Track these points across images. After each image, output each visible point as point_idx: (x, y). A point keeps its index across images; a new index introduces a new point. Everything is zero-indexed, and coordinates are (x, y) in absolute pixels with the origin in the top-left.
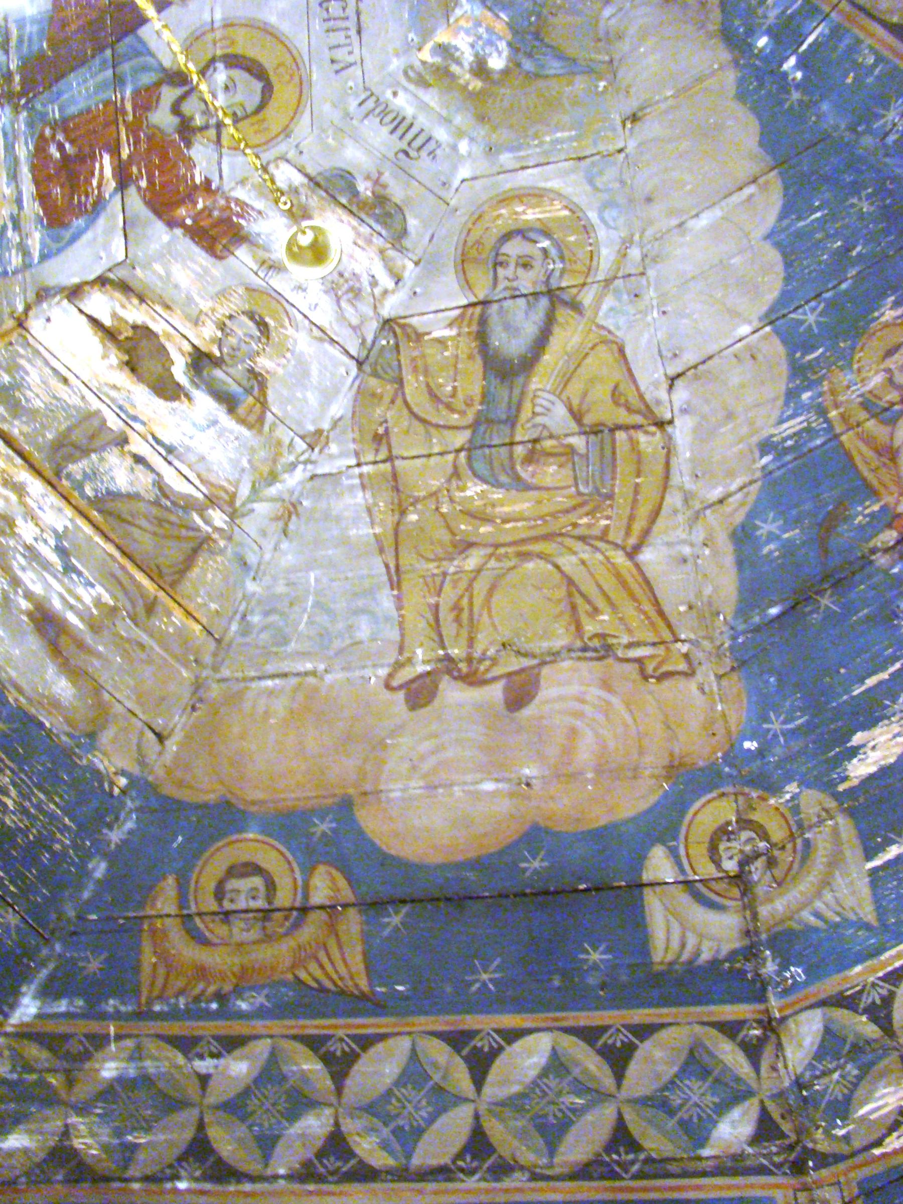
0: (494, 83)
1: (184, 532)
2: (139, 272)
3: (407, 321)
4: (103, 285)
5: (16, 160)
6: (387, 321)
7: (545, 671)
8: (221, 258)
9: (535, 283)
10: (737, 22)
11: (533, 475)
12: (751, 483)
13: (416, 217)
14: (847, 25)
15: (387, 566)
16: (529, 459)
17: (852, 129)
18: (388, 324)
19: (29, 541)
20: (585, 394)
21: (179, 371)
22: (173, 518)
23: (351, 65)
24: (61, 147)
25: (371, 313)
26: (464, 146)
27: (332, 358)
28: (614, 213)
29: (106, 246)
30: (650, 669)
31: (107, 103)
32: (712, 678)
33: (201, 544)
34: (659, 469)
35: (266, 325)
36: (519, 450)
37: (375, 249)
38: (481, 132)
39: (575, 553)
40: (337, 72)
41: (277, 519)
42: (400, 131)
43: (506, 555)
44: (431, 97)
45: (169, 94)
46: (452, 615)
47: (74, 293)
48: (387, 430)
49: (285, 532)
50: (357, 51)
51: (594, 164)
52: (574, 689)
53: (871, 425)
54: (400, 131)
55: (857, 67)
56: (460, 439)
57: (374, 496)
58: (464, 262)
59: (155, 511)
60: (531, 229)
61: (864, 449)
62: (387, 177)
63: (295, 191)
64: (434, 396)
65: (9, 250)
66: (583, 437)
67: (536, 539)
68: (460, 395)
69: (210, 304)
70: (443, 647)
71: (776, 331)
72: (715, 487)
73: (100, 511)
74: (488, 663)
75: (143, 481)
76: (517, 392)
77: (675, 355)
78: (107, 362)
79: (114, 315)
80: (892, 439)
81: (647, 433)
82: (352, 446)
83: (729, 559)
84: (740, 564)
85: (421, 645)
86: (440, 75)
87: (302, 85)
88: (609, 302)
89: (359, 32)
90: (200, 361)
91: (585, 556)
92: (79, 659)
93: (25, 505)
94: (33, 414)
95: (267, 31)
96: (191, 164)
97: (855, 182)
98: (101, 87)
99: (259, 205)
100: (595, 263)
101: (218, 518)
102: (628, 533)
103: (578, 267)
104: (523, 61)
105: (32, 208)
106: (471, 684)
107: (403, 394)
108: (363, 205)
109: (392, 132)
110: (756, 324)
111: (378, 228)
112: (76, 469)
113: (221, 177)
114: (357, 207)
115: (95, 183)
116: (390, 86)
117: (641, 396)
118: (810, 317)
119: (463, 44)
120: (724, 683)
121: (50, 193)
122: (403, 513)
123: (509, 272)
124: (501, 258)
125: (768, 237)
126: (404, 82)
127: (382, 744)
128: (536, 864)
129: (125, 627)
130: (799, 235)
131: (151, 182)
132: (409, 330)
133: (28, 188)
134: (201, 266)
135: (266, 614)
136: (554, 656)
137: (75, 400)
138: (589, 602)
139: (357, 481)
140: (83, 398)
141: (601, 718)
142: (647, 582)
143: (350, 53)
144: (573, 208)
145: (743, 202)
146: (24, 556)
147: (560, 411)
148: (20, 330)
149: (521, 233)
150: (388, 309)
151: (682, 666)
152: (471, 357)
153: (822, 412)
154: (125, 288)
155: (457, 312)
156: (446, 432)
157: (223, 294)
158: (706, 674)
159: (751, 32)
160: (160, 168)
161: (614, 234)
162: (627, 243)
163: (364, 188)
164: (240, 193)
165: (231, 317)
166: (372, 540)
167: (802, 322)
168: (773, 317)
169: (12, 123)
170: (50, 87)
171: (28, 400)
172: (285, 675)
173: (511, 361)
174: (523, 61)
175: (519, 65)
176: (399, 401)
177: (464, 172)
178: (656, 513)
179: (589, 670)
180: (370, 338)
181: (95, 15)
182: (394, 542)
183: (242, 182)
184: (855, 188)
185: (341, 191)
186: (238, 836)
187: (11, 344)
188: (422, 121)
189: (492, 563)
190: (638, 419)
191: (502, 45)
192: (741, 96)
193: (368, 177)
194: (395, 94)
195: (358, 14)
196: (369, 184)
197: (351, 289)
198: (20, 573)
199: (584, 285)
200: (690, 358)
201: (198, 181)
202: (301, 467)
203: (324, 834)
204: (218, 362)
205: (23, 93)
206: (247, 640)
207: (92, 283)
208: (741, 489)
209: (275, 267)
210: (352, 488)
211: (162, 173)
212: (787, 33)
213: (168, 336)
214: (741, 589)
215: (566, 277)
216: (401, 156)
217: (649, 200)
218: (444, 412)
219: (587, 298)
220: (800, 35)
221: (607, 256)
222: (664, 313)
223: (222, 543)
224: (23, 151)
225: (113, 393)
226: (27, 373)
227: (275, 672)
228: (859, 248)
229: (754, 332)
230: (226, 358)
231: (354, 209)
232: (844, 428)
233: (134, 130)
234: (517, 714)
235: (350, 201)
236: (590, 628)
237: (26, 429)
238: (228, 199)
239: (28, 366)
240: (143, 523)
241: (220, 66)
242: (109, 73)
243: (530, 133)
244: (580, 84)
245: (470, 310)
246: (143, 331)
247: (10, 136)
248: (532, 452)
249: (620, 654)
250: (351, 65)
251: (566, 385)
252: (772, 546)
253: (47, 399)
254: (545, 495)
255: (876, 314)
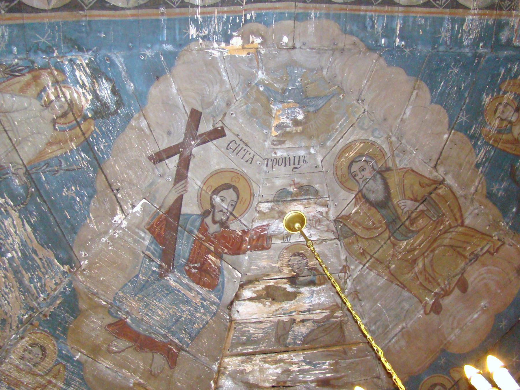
0: (306, 123)
1: (333, 326)
2: (249, 274)
3: (341, 215)
4: (243, 287)
5: (187, 285)
6: (335, 221)
7: (465, 275)
8: (269, 248)
9: (370, 173)
10: (370, 42)
11: (417, 227)
12: (481, 179)
13: (316, 184)
14: (407, 15)
15: (398, 285)
16: (412, 224)
17: (433, 48)
18: (336, 221)
19: (297, 369)
20: (413, 193)
21: (289, 288)
22: (327, 326)
23: (253, 157)
24: (195, 268)
25: (328, 222)
26: (312, 151)
27: (329, 244)
28: (378, 132)
29: (233, 277)
30: (492, 251)
31: (194, 242)
32: (511, 240)
33: (341, 325)
34: (451, 195)
35: (301, 253)
36: (407, 223)
37: (313, 204)
38: (314, 142)
39: (447, 238)
40: (251, 163)
41: (354, 299)
42: (288, 163)
43: (428, 254)
44: (288, 145)
45: (208, 220)
46: (427, 282)
47: (237, 297)
48: (363, 249)
49: (360, 300)
50: (251, 151)
51: (359, 123)
52: (476, 274)
53: (504, 137)
54: (288, 163)
55: (420, 26)
56: (386, 235)
57: (376, 270)
58: (342, 184)
59: (320, 329)
60: (356, 158)
61: (508, 145)
62: (297, 180)
63: (272, 209)
64: (368, 229)
65: (209, 307)
66: (422, 205)
67: (432, 244)
68: (376, 222)
69: (279, 263)
70: (433, 292)
71: (457, 130)
72: (471, 188)
73: (307, 344)
74: (448, 286)
75: (310, 325)
76: (392, 207)
77: (430, 160)
78: (267, 306)
79: (255, 292)
80: (514, 137)
81: (439, 189)
82: (357, 262)
83: (490, 204)
84: (495, 204)
85: (426, 296)
86: (285, 135)
87: (244, 177)
88: (397, 160)
89: (247, 145)
90: (293, 280)
91: (450, 236)
92: (340, 382)
93: (287, 363)
94: (262, 339)
95: (217, 173)
96: (234, 232)
97: (446, 65)
98: (188, 239)
99: (265, 223)
100: (384, 152)
101: (339, 314)
102: (456, 220)
103: (380, 157)
104: (309, 109)
105: (203, 291)
106: (448, 295)
107: (359, 236)
108: (297, 195)
109: (285, 166)
110: (448, 132)
111: (307, 197)
112: (289, 340)
113: (246, 226)
114: (295, 198)
115: (213, 266)
116: (272, 152)
117: (429, 179)
118: (463, 118)
119: (284, 119)
120: (515, 239)
121: (204, 282)
122: (389, 268)
123: (360, 176)
124: (353, 174)
125: (432, 102)
126: (275, 147)
127: (439, 330)
128: (504, 323)
129: (344, 363)
130: (441, 94)
131: (227, 247)
132: (344, 217)
133: (197, 288)
134: (266, 255)
135: (375, 324)
136: (464, 270)
137: (269, 324)
138: (460, 247)
139: (367, 270)
140: (271, 321)
141: (490, 275)
142: (473, 229)
143: (250, 154)
144: (363, 141)
145: (416, 98)
146: (301, 374)
147: (409, 202)
148: (233, 322)
149: (353, 162)
150: (332, 216)
151: (500, 243)
152: (369, 209)
153: (487, 143)
154: (250, 282)
155: (354, 200)
156: (380, 236)
157: (280, 257)
158: (508, 240)
159: (377, 41)
160: (226, 242)
161: (382, 139)
162: (389, 138)
163: (292, 189)
164: (256, 225)
165: (289, 261)
166: (386, 281)
167: (462, 121)
168: (452, 127)
169: (175, 277)
170: (174, 255)
171: (257, 337)
172: (396, 335)
173: (382, 201)
174: (309, 109)
175: (309, 112)
176: (359, 239)
177: (320, 159)
178: (460, 209)
179: (476, 266)
180: (334, 229)
181: (165, 222)
182: (393, 277)
183: (253, 221)
184: (448, 66)
185: (286, 196)
186: (422, 382)
187: (235, 328)
188: (292, 154)
189: (426, 260)
190: (434, 186)
191: (298, 110)
192: (389, 64)
193: (290, 185)
194: (275, 153)
195: (241, 140)
196: (293, 187)
197: (316, 221)
198: (304, 379)
199: (386, 161)
200: (435, 157)
201: (240, 234)
202: (348, 280)
203: (445, 363)
204: (298, 276)
205: (169, 266)
206: (376, 335)
207: (239, 290)
208: (479, 183)
209: (288, 236)
210: (368, 273)
211: (228, 243)
212: (389, 32)
213: (276, 283)
214: (500, 210)
215: (378, 164)
216: (295, 170)
217: (385, 120)
218: (375, 231)
219: (390, 164)
220: (394, 29)
221: (385, 147)
222: (417, 149)
223: (346, 319)
224: (186, 281)
225: (278, 312)
226: (249, 331)
227: (393, 336)
228: (463, 85)
229: (449, 135)
230: (299, 272)
231: (295, 198)
232: (497, 144)
233: (209, 240)
234: (468, 292)
235: (291, 197)
236: (467, 254)
237: (265, 345)
238: (254, 230)
239: (247, 329)
240: (320, 335)
241: (214, 196)
242: (186, 233)
243: (331, 129)
244: (333, 101)
245: (358, 197)
246: (267, 288)
247: (179, 281)
248: (411, 220)
249: (481, 254)
250: (253, 157)
251: (405, 195)
252: (500, 193)
253: (262, 332)
254: (425, 229)
255: (483, 103)
